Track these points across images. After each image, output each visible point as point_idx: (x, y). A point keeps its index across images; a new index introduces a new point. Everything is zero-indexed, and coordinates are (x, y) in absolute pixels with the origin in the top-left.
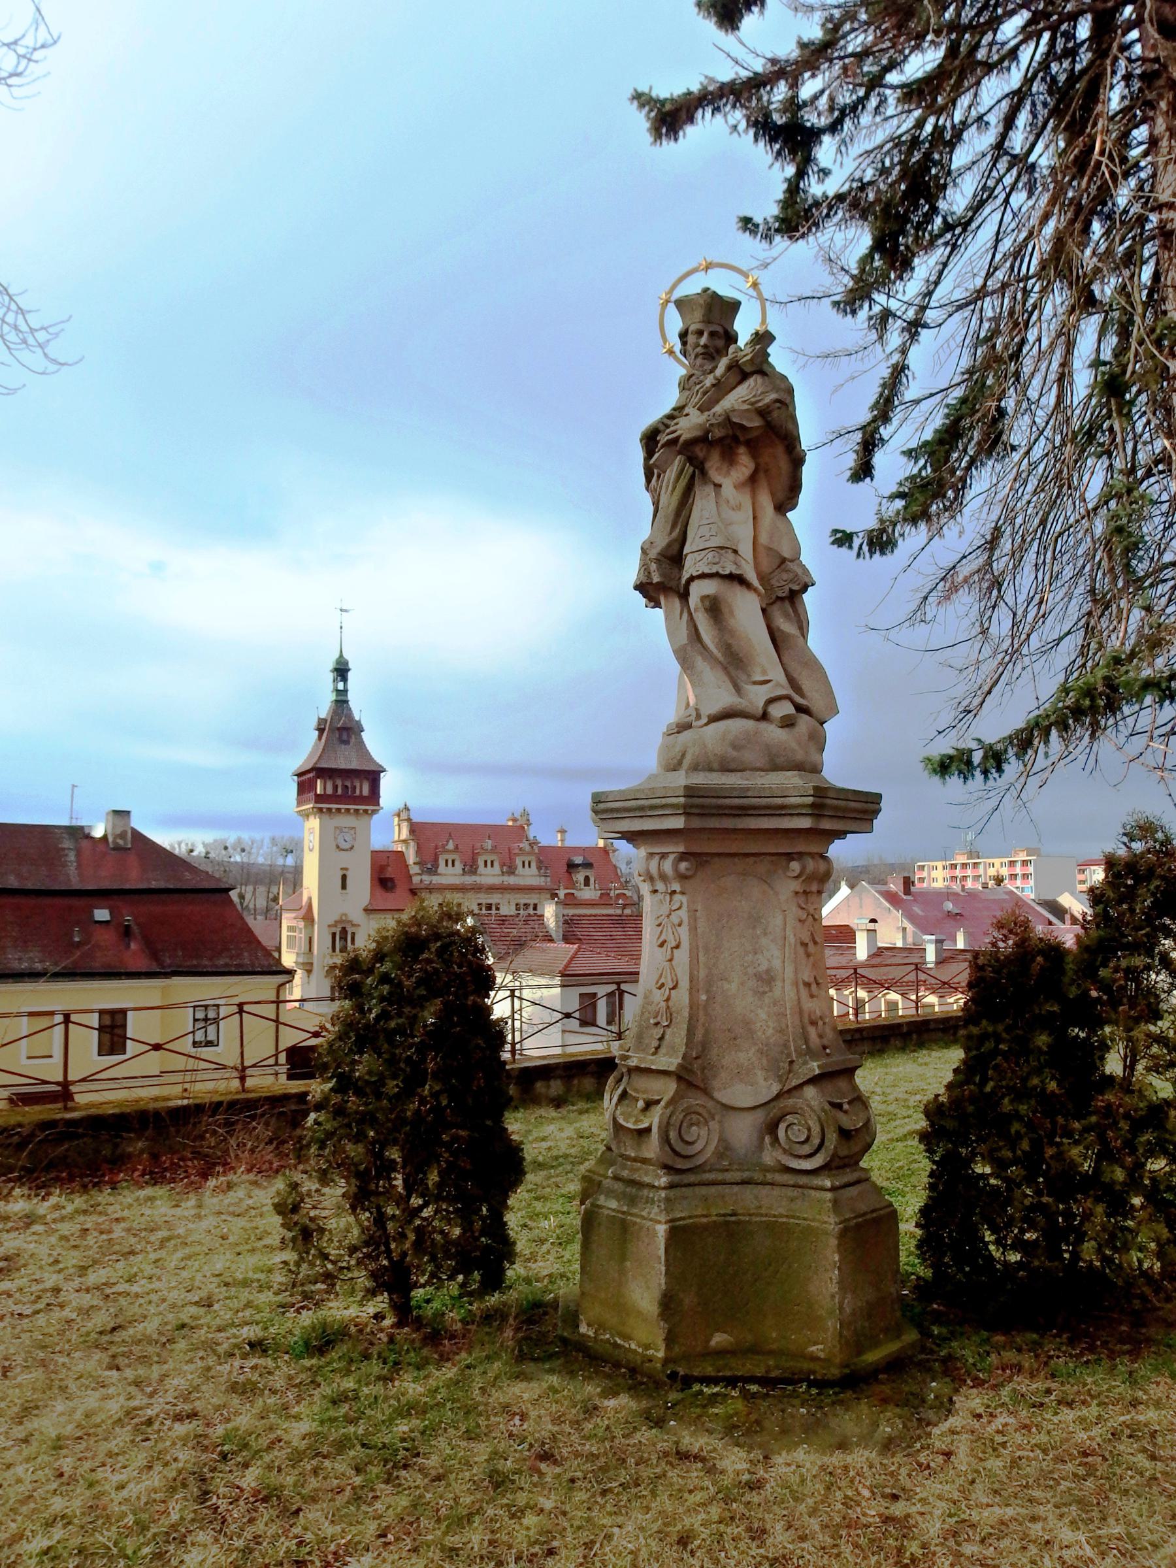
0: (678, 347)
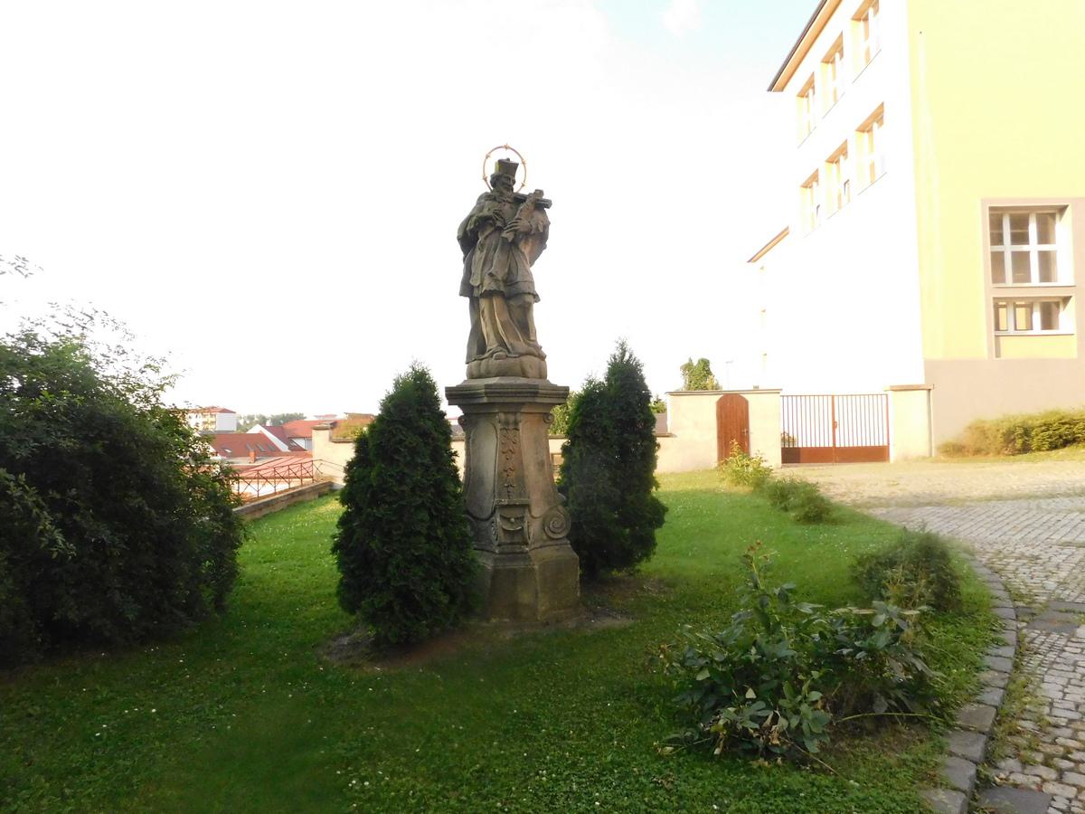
0: (489, 179)
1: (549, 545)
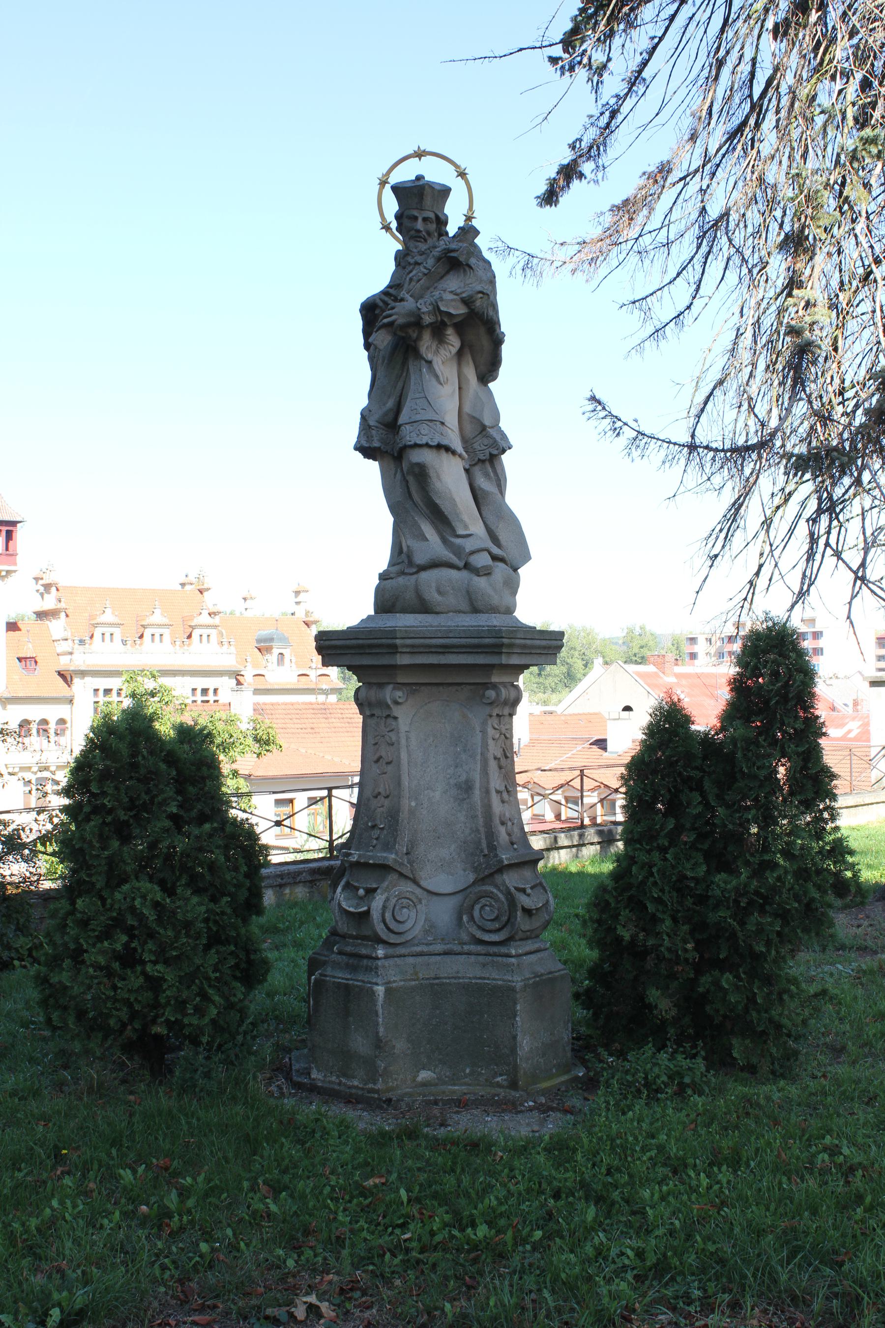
0: (394, 225)
1: (469, 954)
